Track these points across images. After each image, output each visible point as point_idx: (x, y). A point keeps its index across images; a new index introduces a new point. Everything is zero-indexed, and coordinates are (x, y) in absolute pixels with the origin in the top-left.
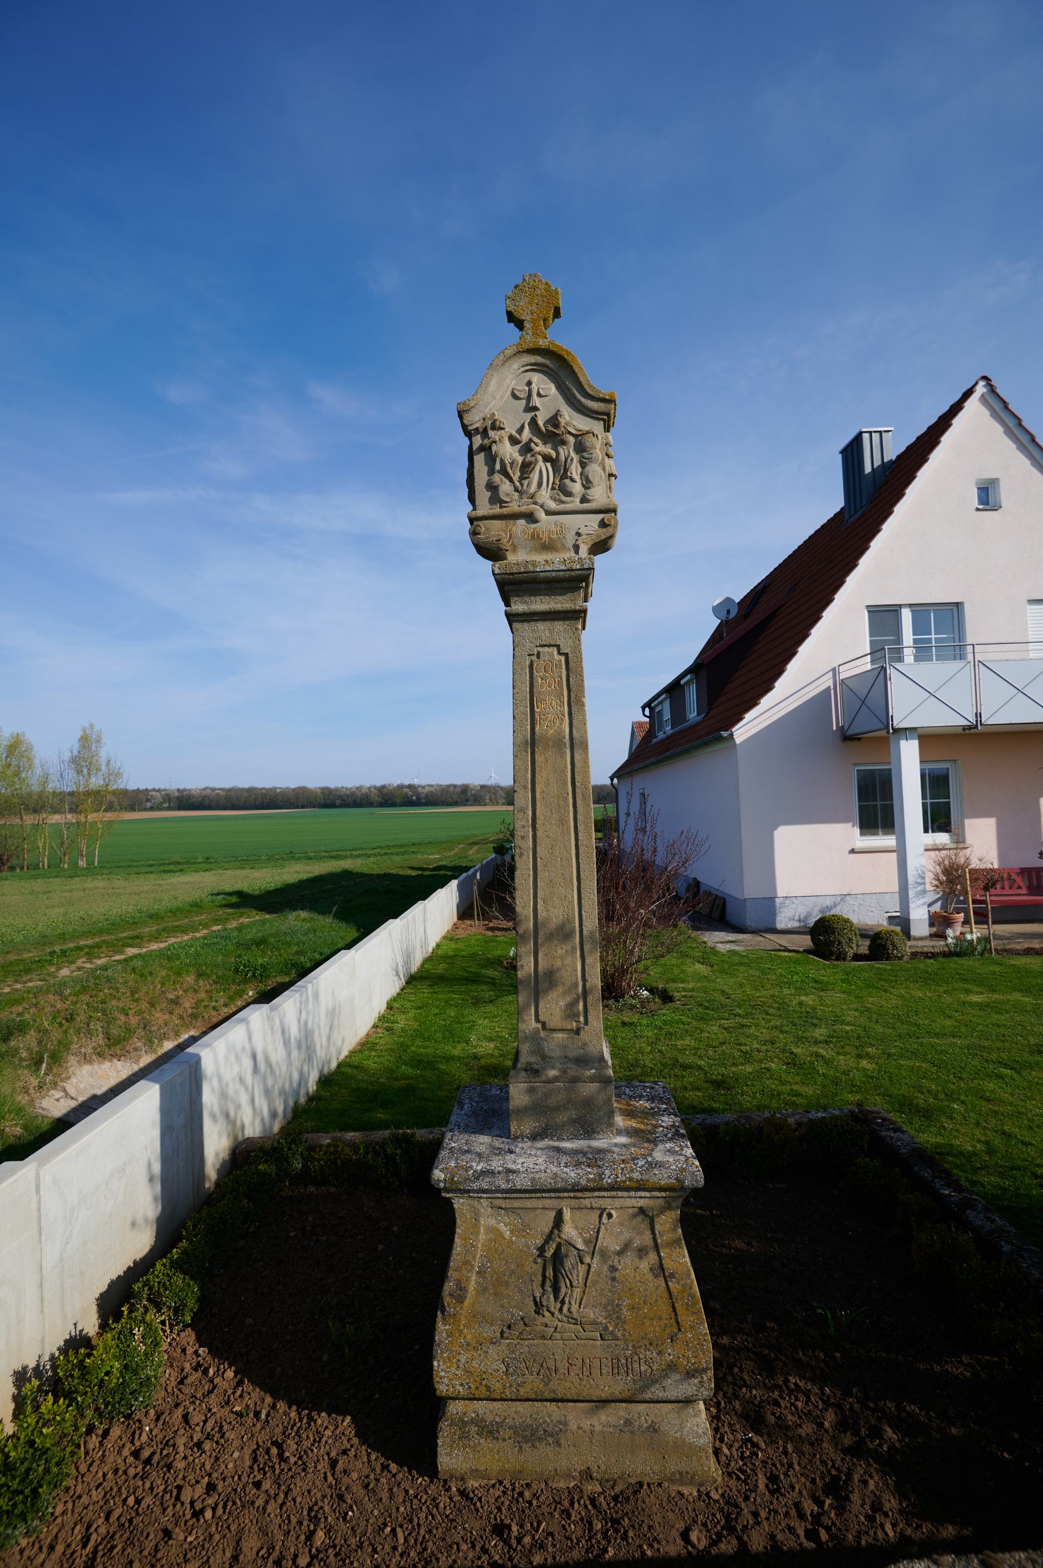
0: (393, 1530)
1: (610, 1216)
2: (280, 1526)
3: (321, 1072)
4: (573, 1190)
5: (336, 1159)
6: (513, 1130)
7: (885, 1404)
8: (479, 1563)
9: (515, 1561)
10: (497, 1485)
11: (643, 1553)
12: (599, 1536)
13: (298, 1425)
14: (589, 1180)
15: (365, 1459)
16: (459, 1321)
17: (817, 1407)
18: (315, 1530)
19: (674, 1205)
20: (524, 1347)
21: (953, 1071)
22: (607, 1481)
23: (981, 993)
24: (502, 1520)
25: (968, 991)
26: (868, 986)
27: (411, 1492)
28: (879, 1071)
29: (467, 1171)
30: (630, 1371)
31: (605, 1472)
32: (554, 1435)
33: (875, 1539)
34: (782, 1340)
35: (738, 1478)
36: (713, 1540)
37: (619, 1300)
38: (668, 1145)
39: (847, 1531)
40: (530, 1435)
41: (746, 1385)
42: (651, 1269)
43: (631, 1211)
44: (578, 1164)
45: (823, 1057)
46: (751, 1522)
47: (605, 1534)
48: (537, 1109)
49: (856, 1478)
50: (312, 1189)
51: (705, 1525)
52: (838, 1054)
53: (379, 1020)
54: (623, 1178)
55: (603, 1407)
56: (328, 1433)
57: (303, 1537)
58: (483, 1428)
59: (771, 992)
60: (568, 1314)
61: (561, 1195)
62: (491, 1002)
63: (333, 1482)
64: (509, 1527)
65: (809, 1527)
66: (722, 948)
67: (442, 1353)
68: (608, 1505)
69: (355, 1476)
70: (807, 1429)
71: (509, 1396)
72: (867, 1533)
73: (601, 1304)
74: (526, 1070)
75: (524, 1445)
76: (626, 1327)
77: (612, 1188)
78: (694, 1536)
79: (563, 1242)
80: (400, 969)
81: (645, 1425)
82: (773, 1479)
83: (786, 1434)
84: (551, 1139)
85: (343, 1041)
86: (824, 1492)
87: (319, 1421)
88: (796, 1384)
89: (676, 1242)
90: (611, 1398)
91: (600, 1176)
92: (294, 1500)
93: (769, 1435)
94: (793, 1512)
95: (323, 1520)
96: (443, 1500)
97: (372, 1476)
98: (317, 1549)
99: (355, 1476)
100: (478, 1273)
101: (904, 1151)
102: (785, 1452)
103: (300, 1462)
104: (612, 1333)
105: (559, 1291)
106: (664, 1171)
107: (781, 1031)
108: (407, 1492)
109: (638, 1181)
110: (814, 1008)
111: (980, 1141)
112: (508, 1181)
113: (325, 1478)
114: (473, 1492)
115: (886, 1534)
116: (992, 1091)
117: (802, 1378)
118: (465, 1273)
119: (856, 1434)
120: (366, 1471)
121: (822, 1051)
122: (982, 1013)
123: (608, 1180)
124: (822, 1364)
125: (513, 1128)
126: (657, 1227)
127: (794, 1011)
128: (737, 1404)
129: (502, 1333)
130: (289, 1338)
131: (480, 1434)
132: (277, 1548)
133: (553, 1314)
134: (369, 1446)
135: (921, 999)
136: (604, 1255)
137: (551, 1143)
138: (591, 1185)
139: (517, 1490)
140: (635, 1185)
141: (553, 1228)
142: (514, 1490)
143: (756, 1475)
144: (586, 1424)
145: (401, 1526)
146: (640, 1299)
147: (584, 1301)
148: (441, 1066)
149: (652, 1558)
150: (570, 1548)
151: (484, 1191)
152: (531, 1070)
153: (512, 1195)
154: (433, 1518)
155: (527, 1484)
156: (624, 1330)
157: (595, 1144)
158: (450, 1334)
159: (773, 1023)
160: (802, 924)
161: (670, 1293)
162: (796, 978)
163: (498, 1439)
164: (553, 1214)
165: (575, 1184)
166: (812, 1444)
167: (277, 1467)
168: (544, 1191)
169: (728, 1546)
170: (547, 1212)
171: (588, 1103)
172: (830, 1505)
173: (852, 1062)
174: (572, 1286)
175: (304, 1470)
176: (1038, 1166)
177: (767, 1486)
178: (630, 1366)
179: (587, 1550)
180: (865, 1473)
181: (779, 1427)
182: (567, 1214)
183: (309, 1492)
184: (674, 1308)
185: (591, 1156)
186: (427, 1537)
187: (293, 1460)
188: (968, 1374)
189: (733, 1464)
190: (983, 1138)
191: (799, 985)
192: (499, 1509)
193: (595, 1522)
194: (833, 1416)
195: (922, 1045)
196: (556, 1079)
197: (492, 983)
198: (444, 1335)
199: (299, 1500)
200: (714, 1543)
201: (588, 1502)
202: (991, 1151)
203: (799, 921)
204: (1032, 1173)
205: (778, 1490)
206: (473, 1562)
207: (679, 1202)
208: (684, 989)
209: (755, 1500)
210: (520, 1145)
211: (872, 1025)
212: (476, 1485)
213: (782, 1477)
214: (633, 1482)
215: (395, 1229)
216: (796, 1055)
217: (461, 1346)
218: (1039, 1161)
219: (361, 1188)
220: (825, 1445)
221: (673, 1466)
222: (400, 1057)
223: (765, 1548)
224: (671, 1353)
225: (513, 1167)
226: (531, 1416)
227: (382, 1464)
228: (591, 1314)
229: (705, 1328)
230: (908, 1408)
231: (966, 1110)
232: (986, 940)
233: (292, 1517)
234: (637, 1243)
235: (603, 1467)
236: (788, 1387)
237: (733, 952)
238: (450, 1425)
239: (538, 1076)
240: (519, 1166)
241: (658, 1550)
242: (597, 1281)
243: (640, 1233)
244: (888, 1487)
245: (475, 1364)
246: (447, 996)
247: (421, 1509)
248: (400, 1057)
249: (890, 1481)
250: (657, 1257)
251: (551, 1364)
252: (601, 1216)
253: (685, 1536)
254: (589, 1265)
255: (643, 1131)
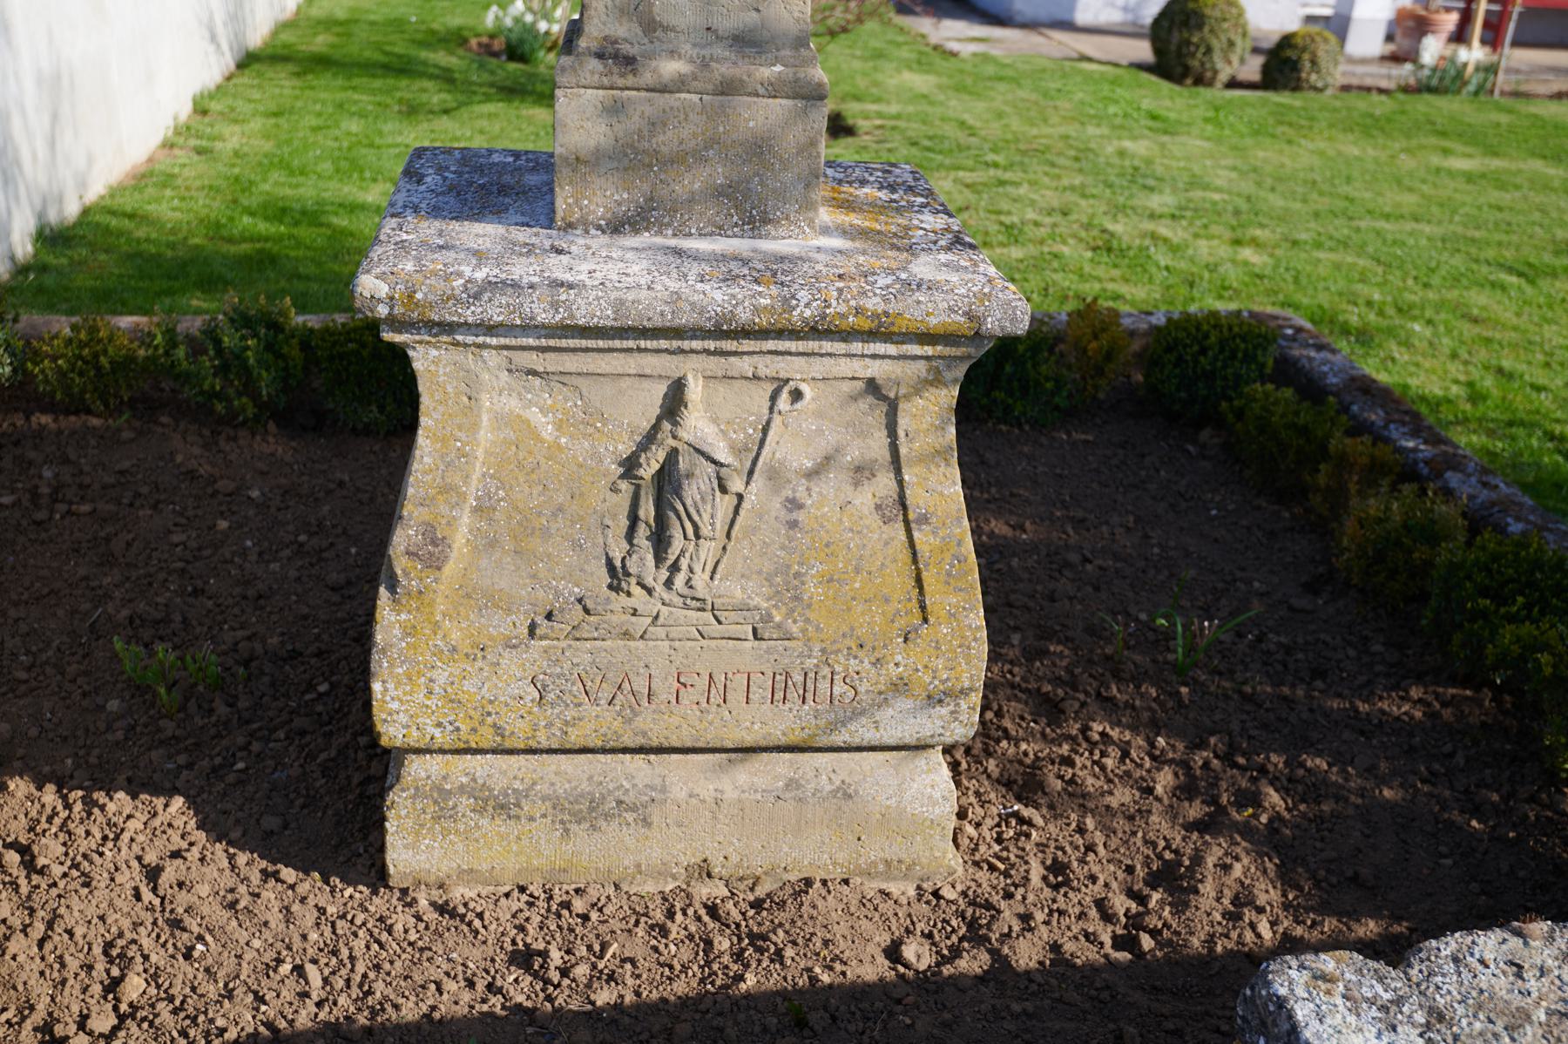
0: (299, 970)
1: (797, 395)
2: (42, 973)
3: (41, 216)
4: (719, 333)
5: (96, 356)
6: (561, 206)
7: (1268, 758)
8: (485, 1008)
9: (560, 1001)
10: (516, 893)
11: (814, 979)
12: (726, 959)
13: (64, 814)
14: (757, 310)
15: (225, 863)
16: (432, 604)
17: (1141, 766)
18: (122, 978)
19: (948, 375)
20: (582, 654)
21: (1414, 273)
22: (741, 879)
23: (1470, 156)
24: (525, 944)
25: (1446, 152)
26: (1256, 133)
27: (331, 910)
28: (1276, 267)
29: (447, 278)
30: (809, 696)
31: (738, 866)
32: (639, 810)
33: (1240, 942)
34: (1078, 671)
35: (992, 868)
36: (943, 956)
37: (801, 564)
38: (943, 257)
39: (1192, 933)
40: (587, 811)
41: (1007, 736)
42: (878, 507)
43: (846, 387)
44: (730, 278)
45: (1166, 240)
46: (1016, 928)
47: (738, 956)
48: (628, 158)
49: (1210, 861)
50: (45, 419)
51: (930, 936)
52: (1196, 236)
53: (177, 132)
54: (842, 309)
55: (742, 761)
56: (134, 825)
57: (97, 989)
58: (486, 801)
59: (1062, 130)
60: (686, 591)
61: (686, 345)
62: (446, 112)
63: (157, 902)
64: (544, 954)
65: (1120, 931)
66: (967, 49)
67: (391, 665)
68: (743, 914)
69: (204, 890)
70: (1123, 796)
71: (545, 744)
72: (1227, 936)
73: (760, 572)
74: (600, 56)
75: (574, 827)
76: (812, 616)
77: (815, 331)
78: (909, 952)
79: (680, 446)
80: (220, 30)
81: (828, 788)
82: (1057, 869)
83: (1083, 806)
84: (660, 233)
85: (90, 160)
86: (1146, 883)
87: (111, 807)
88: (1103, 734)
89: (940, 453)
90: (763, 743)
91: (787, 303)
92: (70, 933)
93: (1051, 807)
94: (1093, 913)
95: (139, 959)
96: (402, 920)
97: (242, 889)
98: (131, 1005)
99: (204, 890)
100: (477, 510)
101: (1335, 380)
102: (1081, 830)
103: (75, 873)
104: (779, 626)
105: (669, 544)
106: (938, 297)
107: (1084, 196)
108: (322, 911)
109: (876, 315)
110: (1149, 162)
111: (1456, 382)
112: (555, 305)
113: (138, 897)
114: (465, 905)
115: (1259, 936)
116: (1484, 308)
117: (1116, 723)
118: (444, 509)
119: (1214, 801)
120: (228, 880)
121: (1163, 231)
122: (1470, 187)
123: (804, 310)
124: (1154, 705)
125: (564, 200)
126: (903, 423)
127: (1108, 164)
128: (992, 765)
129: (532, 629)
130: (23, 675)
131: (480, 811)
132: (40, 1007)
133: (649, 591)
134: (230, 843)
135: (1358, 159)
136: (774, 475)
137: (659, 240)
138: (763, 321)
139: (557, 899)
140: (866, 325)
141: (659, 419)
142: (551, 898)
143: (1027, 863)
144: (707, 790)
145: (314, 961)
146: (848, 562)
147: (728, 561)
148: (335, 220)
149: (831, 986)
150: (669, 978)
151: (492, 329)
152: (616, 56)
153: (564, 343)
154: (381, 946)
155: (577, 891)
156: (807, 621)
157: (767, 245)
158: (409, 631)
159: (1065, 182)
160: (1130, 17)
161: (914, 554)
162: (1112, 109)
163: (518, 817)
164: (661, 389)
165: (721, 319)
166: (1131, 818)
167: (23, 882)
168: (645, 333)
169: (973, 963)
170: (646, 384)
171: (759, 149)
172: (1162, 902)
173: (1224, 251)
174: (698, 537)
175: (86, 885)
176: (1558, 421)
177: (1044, 878)
178: (810, 686)
179: (702, 981)
180: (1226, 854)
181: (1070, 795)
182: (695, 391)
183: (102, 918)
184: (919, 581)
185: (760, 266)
186: (372, 975)
187: (57, 870)
188: (1418, 714)
189: (983, 848)
190: (1462, 378)
191: (1118, 121)
192: (521, 929)
193: (717, 939)
194: (1170, 777)
195: (1358, 230)
196: (679, 85)
197: (446, 78)
198: (397, 632)
199: (79, 931)
200: (944, 960)
201: (702, 912)
202: (1476, 397)
203: (1125, 9)
204: (1545, 433)
205: (1067, 883)
206: (472, 1007)
207: (960, 371)
208: (880, 115)
209: (1024, 898)
210: (581, 241)
211: (1262, 194)
212: (473, 894)
213: (1075, 864)
214: (793, 878)
215: (255, 494)
216: (1112, 235)
217: (438, 653)
218: (1559, 414)
219: (164, 419)
220: (1154, 818)
221: (875, 850)
222: (235, 201)
223: (1041, 963)
224: (901, 660)
225: (568, 277)
226: (590, 778)
227: (264, 872)
228: (732, 589)
229: (978, 618)
230: (1309, 763)
231: (1436, 334)
232: (1491, 69)
233: (68, 958)
234: (852, 455)
235: (734, 858)
236: (1087, 739)
237: (985, 58)
238: (414, 797)
239: (634, 72)
240: (584, 277)
241: (844, 973)
242: (755, 530)
243: (862, 434)
244: (1265, 872)
245: (467, 685)
246: (340, 96)
247: (355, 935)
248: (235, 201)
249: (1269, 865)
250: (894, 485)
251: (641, 685)
252: (774, 398)
253: (893, 953)
254: (740, 497)
255: (879, 232)
